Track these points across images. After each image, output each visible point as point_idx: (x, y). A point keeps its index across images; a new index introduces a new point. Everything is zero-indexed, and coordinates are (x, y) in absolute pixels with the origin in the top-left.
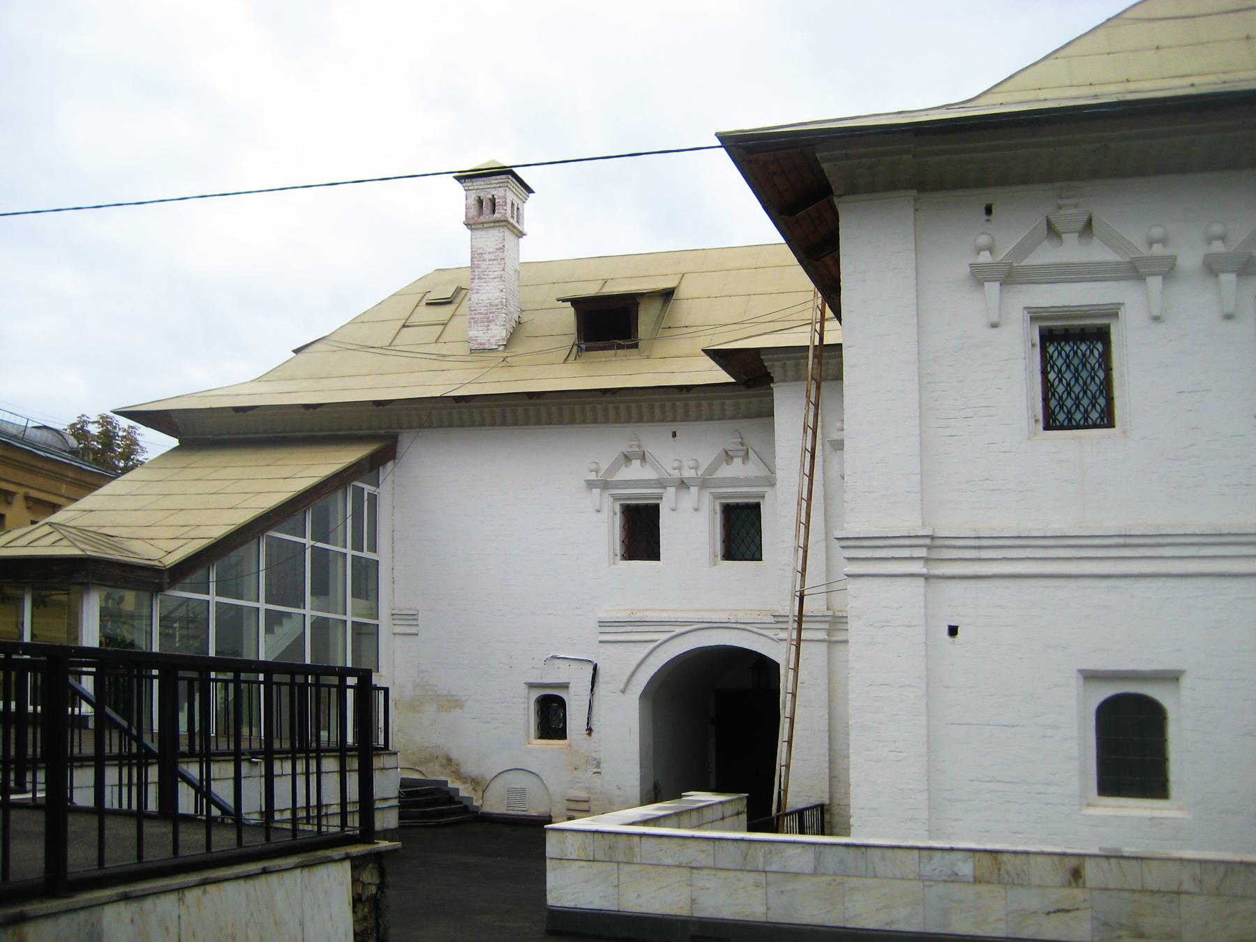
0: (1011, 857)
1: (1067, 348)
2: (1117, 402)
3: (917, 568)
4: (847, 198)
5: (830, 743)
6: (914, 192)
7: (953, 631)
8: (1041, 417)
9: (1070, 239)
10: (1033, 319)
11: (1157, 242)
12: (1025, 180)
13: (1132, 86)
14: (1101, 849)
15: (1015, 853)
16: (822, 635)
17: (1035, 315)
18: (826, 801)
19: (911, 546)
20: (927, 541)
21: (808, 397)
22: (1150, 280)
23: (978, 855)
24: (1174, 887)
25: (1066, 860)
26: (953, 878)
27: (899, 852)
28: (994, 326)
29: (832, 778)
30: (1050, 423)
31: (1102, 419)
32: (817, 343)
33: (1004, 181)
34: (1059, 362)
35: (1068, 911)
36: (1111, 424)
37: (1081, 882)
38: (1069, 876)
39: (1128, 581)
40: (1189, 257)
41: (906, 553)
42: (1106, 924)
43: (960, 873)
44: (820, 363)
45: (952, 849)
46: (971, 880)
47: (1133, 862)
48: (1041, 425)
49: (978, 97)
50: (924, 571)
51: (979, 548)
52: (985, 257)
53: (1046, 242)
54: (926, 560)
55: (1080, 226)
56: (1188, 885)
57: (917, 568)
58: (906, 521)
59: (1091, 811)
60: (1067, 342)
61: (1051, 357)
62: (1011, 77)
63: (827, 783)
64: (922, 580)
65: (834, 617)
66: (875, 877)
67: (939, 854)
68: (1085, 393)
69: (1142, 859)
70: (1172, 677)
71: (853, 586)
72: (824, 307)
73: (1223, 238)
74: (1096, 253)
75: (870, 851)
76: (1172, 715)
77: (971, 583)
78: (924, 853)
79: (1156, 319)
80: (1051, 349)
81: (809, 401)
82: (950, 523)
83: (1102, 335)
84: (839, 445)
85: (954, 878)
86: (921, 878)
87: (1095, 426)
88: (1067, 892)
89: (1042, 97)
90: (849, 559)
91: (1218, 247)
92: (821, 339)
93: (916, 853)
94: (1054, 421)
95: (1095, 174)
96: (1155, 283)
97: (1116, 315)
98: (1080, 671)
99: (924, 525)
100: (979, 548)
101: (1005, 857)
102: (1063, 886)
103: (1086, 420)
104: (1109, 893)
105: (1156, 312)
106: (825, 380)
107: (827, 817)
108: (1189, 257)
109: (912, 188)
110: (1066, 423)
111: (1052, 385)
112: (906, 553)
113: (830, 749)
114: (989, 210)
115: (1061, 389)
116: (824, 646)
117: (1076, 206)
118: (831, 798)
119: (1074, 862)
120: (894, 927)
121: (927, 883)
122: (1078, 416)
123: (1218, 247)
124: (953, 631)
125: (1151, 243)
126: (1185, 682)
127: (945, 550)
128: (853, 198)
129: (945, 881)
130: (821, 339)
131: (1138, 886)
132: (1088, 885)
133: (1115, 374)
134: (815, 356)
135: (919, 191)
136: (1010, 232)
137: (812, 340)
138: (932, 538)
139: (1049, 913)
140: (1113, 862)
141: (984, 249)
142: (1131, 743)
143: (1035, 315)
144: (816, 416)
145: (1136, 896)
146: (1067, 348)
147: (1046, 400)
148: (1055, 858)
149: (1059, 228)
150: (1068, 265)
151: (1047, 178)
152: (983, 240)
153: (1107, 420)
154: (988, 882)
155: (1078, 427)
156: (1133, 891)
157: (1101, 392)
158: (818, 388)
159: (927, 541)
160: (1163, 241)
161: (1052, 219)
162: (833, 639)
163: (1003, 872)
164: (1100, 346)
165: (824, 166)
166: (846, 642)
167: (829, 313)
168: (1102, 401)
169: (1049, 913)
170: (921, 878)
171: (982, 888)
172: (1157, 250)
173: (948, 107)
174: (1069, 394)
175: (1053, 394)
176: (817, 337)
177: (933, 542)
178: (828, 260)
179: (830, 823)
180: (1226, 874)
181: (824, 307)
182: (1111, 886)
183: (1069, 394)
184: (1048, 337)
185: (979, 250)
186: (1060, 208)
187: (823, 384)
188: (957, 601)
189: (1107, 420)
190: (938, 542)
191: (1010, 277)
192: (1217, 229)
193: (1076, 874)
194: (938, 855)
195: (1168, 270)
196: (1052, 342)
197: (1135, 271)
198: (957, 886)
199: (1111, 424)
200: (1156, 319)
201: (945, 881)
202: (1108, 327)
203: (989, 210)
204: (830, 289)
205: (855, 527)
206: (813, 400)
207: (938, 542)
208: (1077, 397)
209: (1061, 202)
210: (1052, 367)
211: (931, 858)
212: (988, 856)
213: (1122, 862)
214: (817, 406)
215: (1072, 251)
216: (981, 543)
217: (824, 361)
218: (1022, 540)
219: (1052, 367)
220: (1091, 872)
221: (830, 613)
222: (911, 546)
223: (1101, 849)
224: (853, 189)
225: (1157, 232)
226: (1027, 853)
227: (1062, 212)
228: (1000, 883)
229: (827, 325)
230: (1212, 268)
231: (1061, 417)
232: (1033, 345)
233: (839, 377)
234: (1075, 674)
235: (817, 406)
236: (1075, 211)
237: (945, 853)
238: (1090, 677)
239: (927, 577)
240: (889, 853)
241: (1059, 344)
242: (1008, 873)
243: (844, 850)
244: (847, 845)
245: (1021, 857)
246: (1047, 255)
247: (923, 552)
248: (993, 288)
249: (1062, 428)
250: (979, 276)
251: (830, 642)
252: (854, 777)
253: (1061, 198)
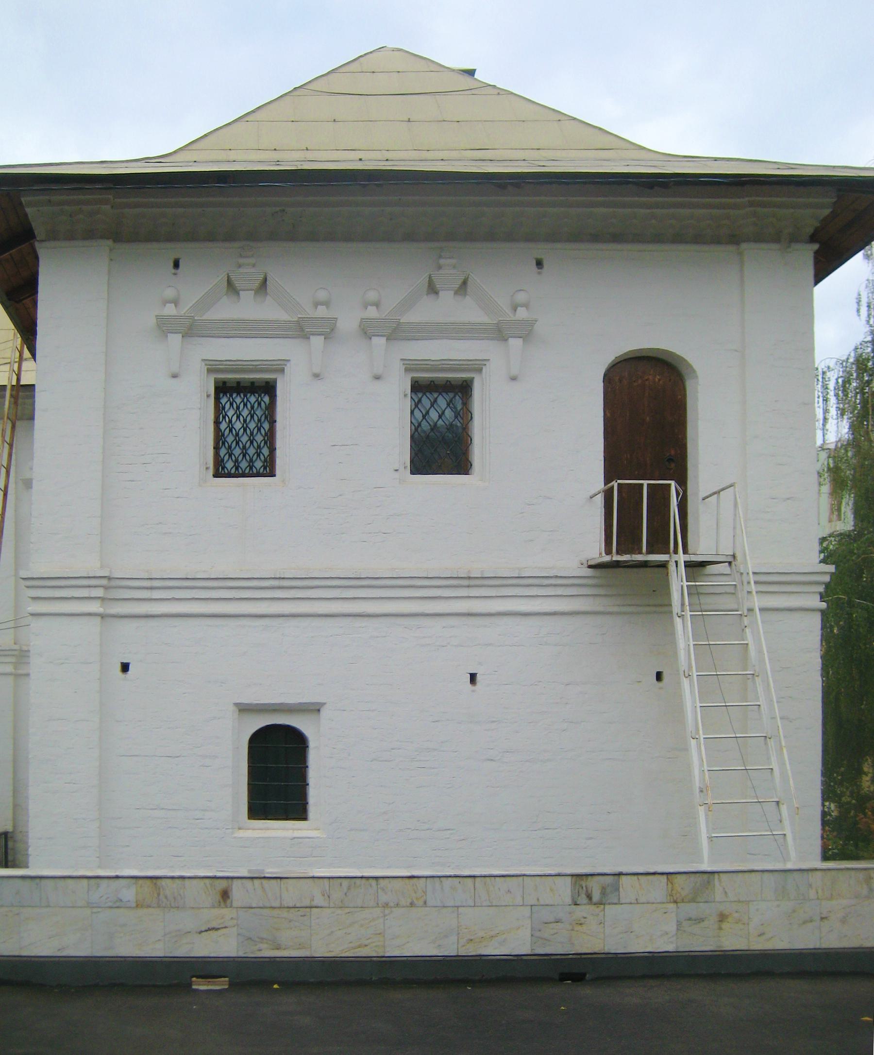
0: (169, 881)
1: (238, 400)
2: (278, 453)
3: (95, 607)
4: (47, 244)
5: (15, 772)
6: (110, 243)
7: (125, 667)
8: (211, 464)
9: (247, 296)
10: (209, 371)
11: (322, 304)
12: (211, 237)
13: (310, 155)
14: (250, 871)
15: (173, 878)
16: (9, 669)
17: (212, 368)
18: (10, 828)
19: (89, 587)
20: (104, 582)
21: (3, 436)
22: (313, 339)
23: (141, 882)
24: (307, 903)
25: (217, 882)
26: (118, 904)
27: (70, 881)
28: (175, 376)
29: (16, 806)
30: (220, 472)
31: (265, 468)
32: (14, 383)
33: (193, 237)
34: (231, 413)
35: (217, 929)
36: (272, 474)
37: (229, 902)
38: (218, 897)
39: (281, 620)
40: (348, 321)
41: (84, 593)
42: (250, 939)
43: (124, 900)
44: (16, 403)
45: (117, 877)
46: (134, 905)
47: (273, 881)
48: (211, 472)
49: (175, 152)
50: (101, 610)
51: (151, 588)
52: (170, 310)
53: (225, 299)
54: (102, 599)
55: (257, 284)
56: (319, 900)
57: (95, 607)
58: (87, 563)
59: (241, 834)
60: (238, 394)
61: (224, 408)
62: (205, 136)
63: (11, 811)
64: (99, 619)
65: (21, 651)
66: (48, 906)
67: (106, 881)
68: (252, 443)
69: (281, 878)
70: (314, 709)
71: (36, 625)
72: (22, 347)
73: (377, 305)
74: (267, 310)
75: (44, 882)
76: (312, 744)
77: (142, 622)
78: (93, 881)
79: (316, 376)
80: (224, 400)
81: (4, 441)
82: (129, 564)
83: (269, 389)
84: (28, 484)
85: (118, 904)
86: (90, 905)
87: (258, 475)
88: (216, 912)
89: (232, 158)
90: (34, 598)
91: (372, 312)
92: (18, 380)
93: (85, 881)
94: (223, 468)
95: (273, 236)
96: (317, 341)
97: (282, 371)
98: (236, 704)
99: (102, 567)
100: (151, 588)
101: (163, 882)
102: (213, 907)
103: (251, 468)
104: (253, 910)
105: (316, 370)
106: (21, 419)
107: (10, 844)
108: (348, 321)
109: (108, 239)
110: (233, 471)
111: (223, 435)
112: (84, 593)
113: (14, 779)
114: (176, 265)
115: (230, 439)
116: (11, 679)
117: (254, 266)
118: (14, 826)
119: (224, 884)
120: (64, 954)
121: (95, 910)
122: (244, 465)
123: (372, 312)
124: (125, 667)
125: (316, 304)
126: (324, 712)
127: (121, 591)
128: (52, 244)
129: (111, 907)
130: (18, 380)
131: (277, 904)
132: (235, 904)
133: (279, 426)
134: (11, 396)
135: (114, 241)
136: (194, 286)
137: (10, 379)
138: (109, 578)
139: (201, 932)
140: (256, 882)
141: (170, 302)
142: (277, 772)
143: (212, 368)
144: (10, 455)
145: (276, 912)
146: (238, 400)
147: (217, 448)
148: (207, 881)
149: (237, 284)
150: (244, 321)
151: (230, 237)
152: (170, 293)
153: (269, 469)
154: (149, 906)
155: (244, 475)
156: (274, 908)
157: (266, 443)
158: (13, 427)
159: (104, 582)
160: (327, 304)
161: (233, 278)
162: (20, 672)
163: (161, 896)
164: (267, 399)
165: (29, 210)
166: (28, 675)
167: (27, 354)
168: (266, 451)
169: (201, 932)
170: (90, 905)
171: (141, 912)
172: (321, 312)
173: (147, 160)
174: (237, 443)
175: (223, 443)
176: (15, 377)
177: (109, 582)
178: (27, 302)
179: (13, 849)
180: (349, 888)
181: (22, 347)
182: (254, 905)
183: (237, 443)
184: (222, 389)
185: (165, 302)
186: (240, 266)
187: (18, 424)
188: (130, 639)
189: (269, 469)
190: (114, 583)
191: (191, 330)
192: (372, 296)
193: (225, 895)
194: (104, 883)
195: (329, 331)
196: (225, 394)
197: (301, 330)
198: (122, 910)
199: (272, 474)
200: (316, 376)
201: (111, 907)
202: (275, 381)
203: (176, 265)
204: (27, 329)
205: (39, 567)
206: (8, 439)
207: (114, 583)
208: (244, 447)
209: (241, 261)
210: (224, 418)
211: (98, 886)
212: (148, 882)
213: (264, 881)
214: (11, 446)
215: (247, 308)
216: (153, 584)
217: (20, 401)
218: (189, 581)
219: (224, 418)
220: (238, 892)
221: (16, 647)
222: (89, 587)
223: (250, 871)
224: (53, 236)
225: (322, 295)
226: (183, 878)
227: (241, 270)
228: (159, 907)
229: (25, 365)
230: (367, 331)
231: (230, 465)
232: (208, 396)
233: (32, 418)
234: (232, 708)
235: (11, 446)
236: (253, 270)
237: (111, 881)
238: (245, 709)
239: (103, 616)
240: (61, 883)
241: (231, 396)
242: (166, 897)
243: (19, 882)
244: (23, 877)
245: (177, 881)
246: (227, 310)
247: (100, 592)
248: (175, 339)
249: (229, 475)
250: (164, 327)
251: (17, 676)
252: (33, 808)
253: (241, 256)
